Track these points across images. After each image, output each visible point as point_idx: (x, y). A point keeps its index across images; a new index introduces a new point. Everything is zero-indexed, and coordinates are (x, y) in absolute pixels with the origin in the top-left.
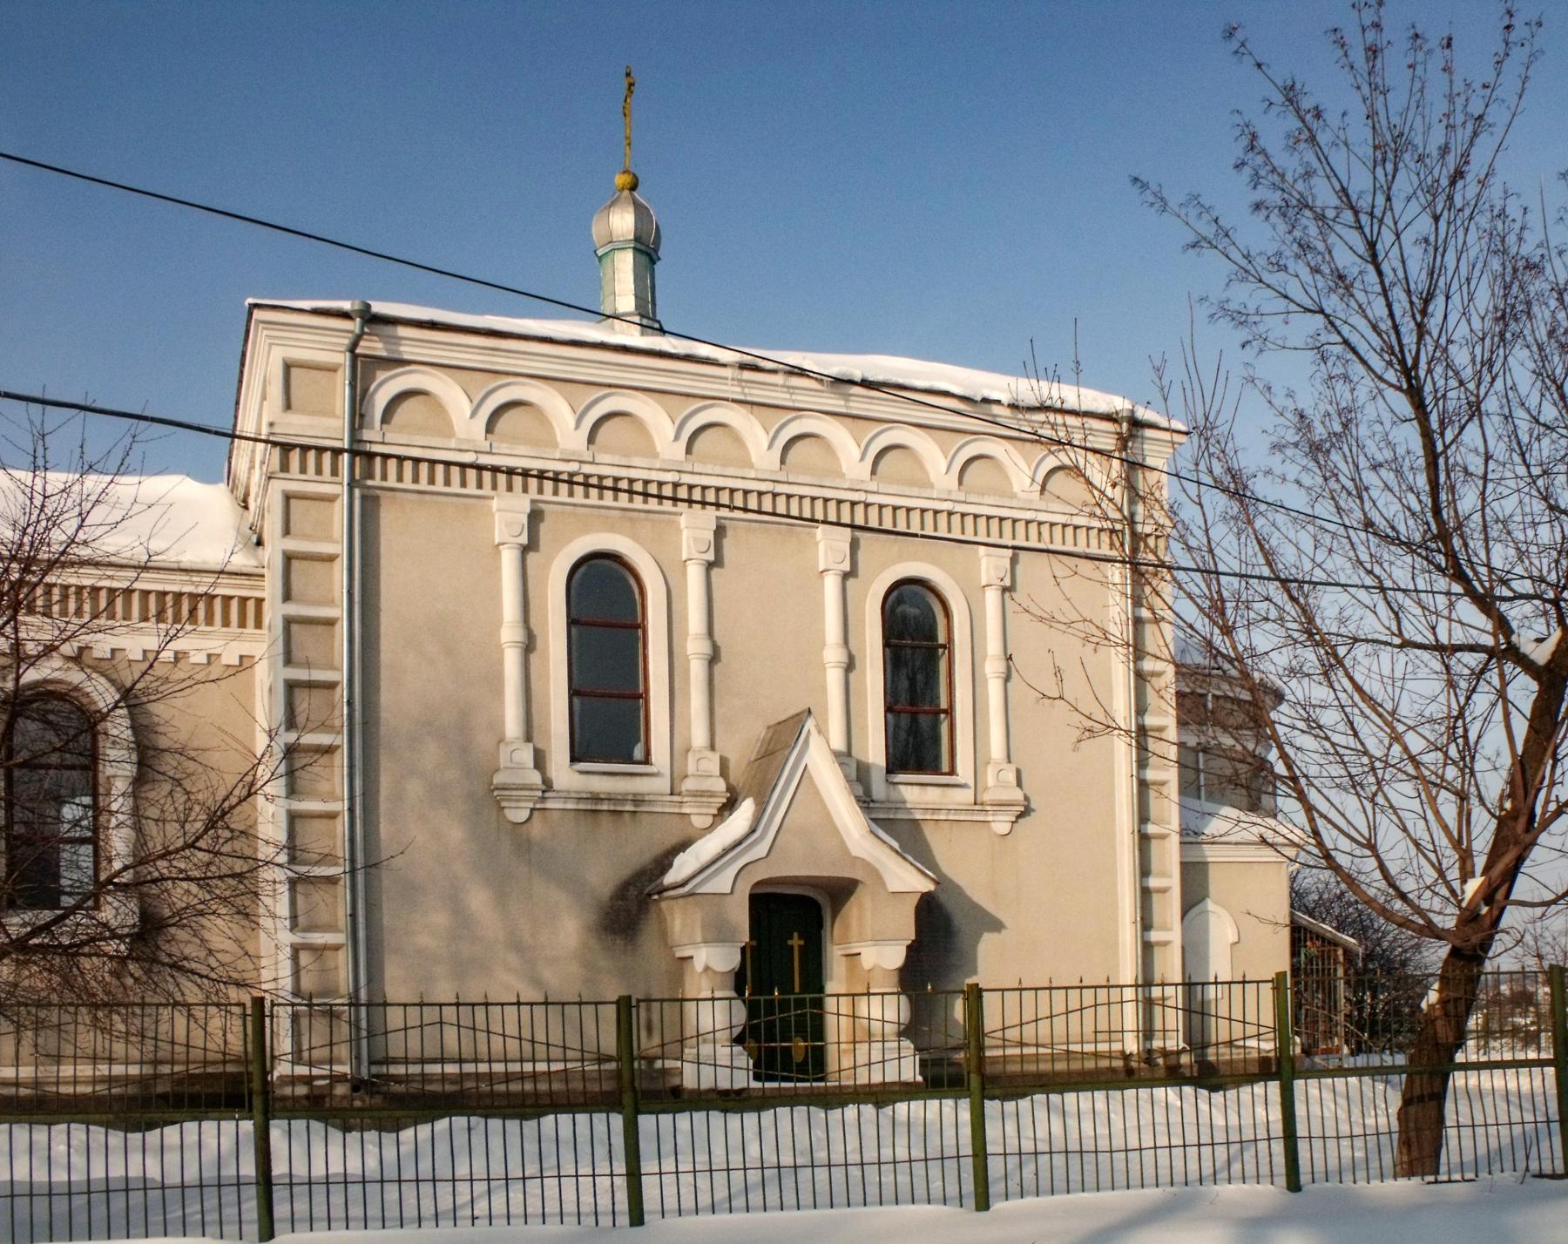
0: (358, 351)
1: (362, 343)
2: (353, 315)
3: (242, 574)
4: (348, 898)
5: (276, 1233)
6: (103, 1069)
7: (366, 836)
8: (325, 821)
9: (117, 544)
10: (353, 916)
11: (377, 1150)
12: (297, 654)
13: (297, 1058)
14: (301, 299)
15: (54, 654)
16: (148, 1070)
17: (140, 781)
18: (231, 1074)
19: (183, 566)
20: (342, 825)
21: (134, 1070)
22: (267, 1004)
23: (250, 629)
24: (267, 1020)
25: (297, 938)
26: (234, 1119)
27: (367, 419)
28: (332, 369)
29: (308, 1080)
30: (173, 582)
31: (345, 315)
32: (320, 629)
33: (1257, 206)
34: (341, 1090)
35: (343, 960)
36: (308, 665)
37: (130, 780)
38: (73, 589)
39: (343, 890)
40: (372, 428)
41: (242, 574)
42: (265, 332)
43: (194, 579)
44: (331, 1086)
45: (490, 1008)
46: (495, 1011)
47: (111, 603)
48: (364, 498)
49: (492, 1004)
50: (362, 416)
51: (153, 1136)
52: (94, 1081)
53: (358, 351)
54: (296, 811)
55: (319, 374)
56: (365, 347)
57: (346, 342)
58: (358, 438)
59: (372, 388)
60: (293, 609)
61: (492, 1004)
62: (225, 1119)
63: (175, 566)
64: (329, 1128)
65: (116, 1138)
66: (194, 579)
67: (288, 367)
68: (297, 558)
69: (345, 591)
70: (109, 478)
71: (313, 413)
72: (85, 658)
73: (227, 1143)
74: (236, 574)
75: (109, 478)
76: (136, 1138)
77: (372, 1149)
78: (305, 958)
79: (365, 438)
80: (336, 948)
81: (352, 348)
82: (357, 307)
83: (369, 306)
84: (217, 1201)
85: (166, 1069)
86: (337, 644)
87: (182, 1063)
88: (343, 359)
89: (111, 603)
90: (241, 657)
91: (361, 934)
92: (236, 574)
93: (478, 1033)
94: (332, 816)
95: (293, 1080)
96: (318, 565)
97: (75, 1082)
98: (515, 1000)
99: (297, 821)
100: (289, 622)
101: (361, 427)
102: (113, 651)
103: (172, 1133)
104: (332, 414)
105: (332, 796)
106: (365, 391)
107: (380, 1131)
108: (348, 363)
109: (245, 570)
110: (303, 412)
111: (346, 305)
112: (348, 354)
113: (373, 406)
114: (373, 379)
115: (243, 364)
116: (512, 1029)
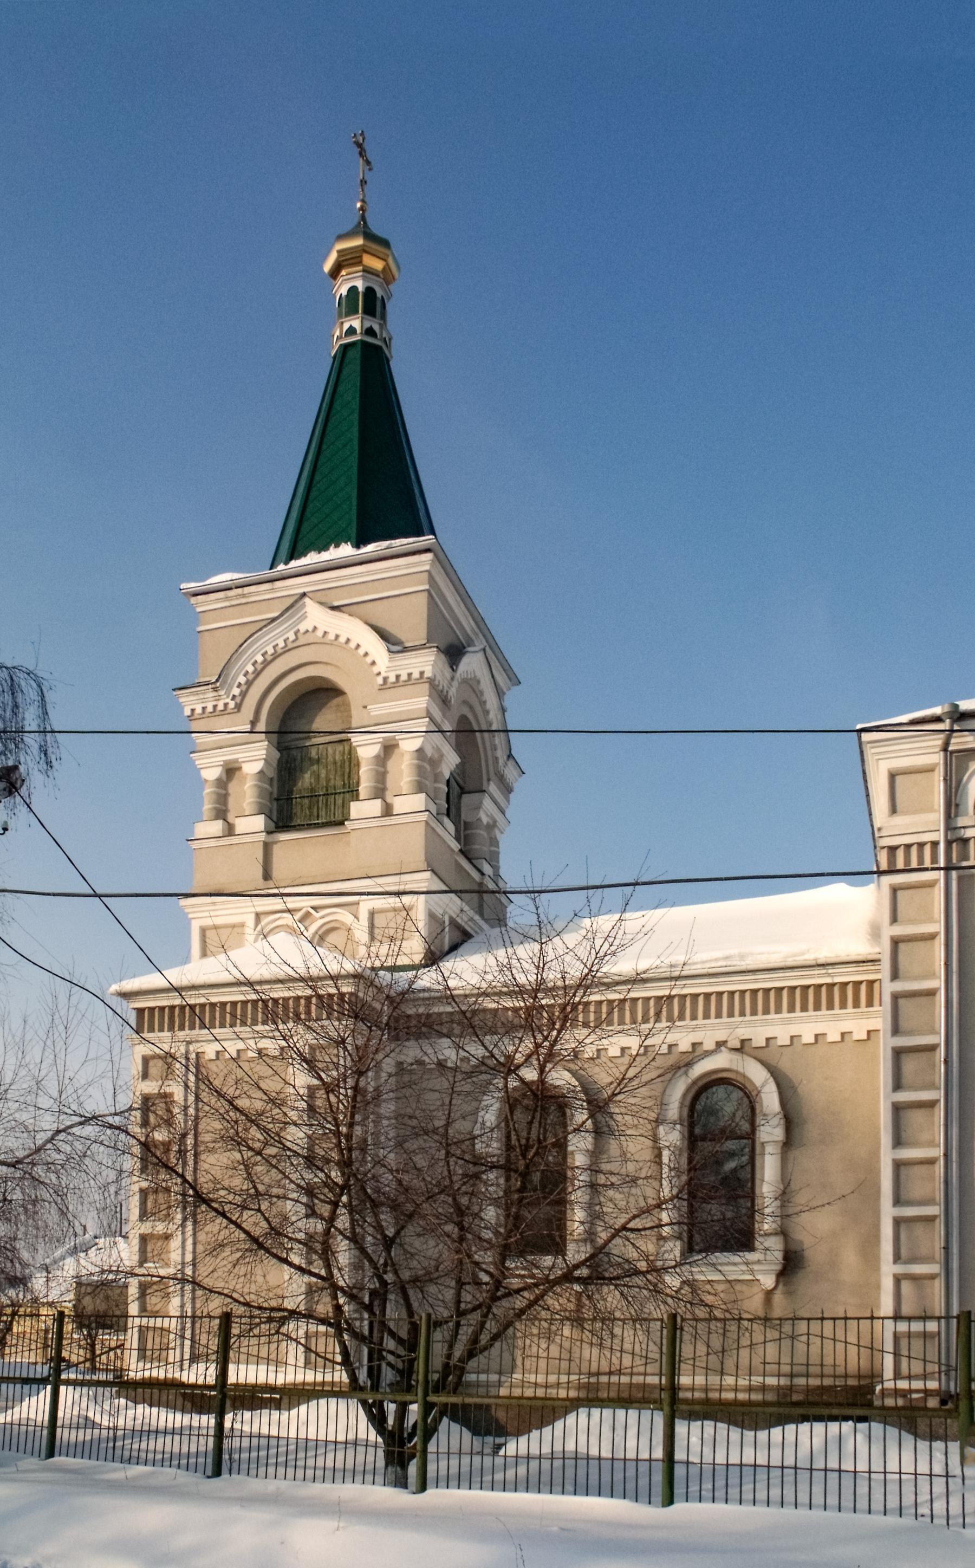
0: (950, 748)
1: (953, 741)
2: (943, 717)
3: (868, 961)
4: (942, 1233)
5: (675, 1499)
6: (757, 1380)
7: (961, 1178)
8: (926, 1166)
9: (622, 966)
10: (947, 1248)
11: (944, 1457)
12: (903, 1024)
13: (897, 1375)
14: (897, 715)
15: (723, 1048)
16: (784, 1381)
17: (788, 1144)
18: (852, 1387)
19: (820, 962)
20: (940, 1168)
21: (772, 1381)
22: (679, 1319)
23: (850, 1010)
24: (678, 1332)
25: (900, 1269)
26: (650, 1408)
27: (961, 807)
28: (930, 770)
29: (904, 1394)
30: (811, 976)
31: (938, 719)
32: (923, 1000)
33: (315, 628)
34: (933, 1403)
35: (938, 1286)
36: (910, 1033)
37: (781, 1144)
38: (616, 1003)
39: (940, 1226)
40: (966, 814)
41: (868, 961)
42: (873, 751)
43: (830, 971)
44: (925, 1399)
45: (848, 1321)
46: (852, 1324)
47: (610, 1013)
48: (960, 878)
49: (850, 1318)
50: (957, 805)
51: (762, 1435)
52: (750, 1389)
53: (950, 748)
54: (900, 1160)
55: (919, 776)
56: (957, 743)
57: (940, 742)
58: (954, 826)
59: (965, 778)
60: (899, 986)
61: (850, 1318)
62: (643, 1409)
63: (813, 963)
64: (903, 1433)
65: (735, 1433)
66: (830, 971)
67: (892, 776)
68: (903, 941)
69: (942, 963)
70: (617, 916)
71: (915, 812)
72: (746, 1049)
73: (818, 1442)
74: (864, 962)
75: (617, 916)
76: (749, 1434)
77: (939, 1456)
78: (906, 1287)
79: (959, 825)
80: (932, 1277)
81: (945, 749)
82: (946, 710)
83: (957, 706)
84: (724, 1482)
85: (802, 1381)
86: (937, 1007)
87: (816, 1376)
88: (938, 758)
89: (610, 1013)
90: (869, 1032)
91: (955, 1264)
92: (864, 962)
93: (837, 1343)
94: (931, 1162)
95: (897, 1392)
96: (921, 944)
97: (736, 1390)
98: (869, 1315)
99: (902, 1168)
100: (896, 997)
101: (956, 816)
102: (768, 1040)
103: (776, 1432)
104: (931, 810)
105: (932, 1144)
106: (959, 782)
107: (931, 1441)
108: (942, 762)
109: (870, 957)
110: (906, 813)
111: (937, 710)
112: (942, 753)
113: (967, 794)
114: (967, 769)
115: (866, 781)
116: (852, 1338)
